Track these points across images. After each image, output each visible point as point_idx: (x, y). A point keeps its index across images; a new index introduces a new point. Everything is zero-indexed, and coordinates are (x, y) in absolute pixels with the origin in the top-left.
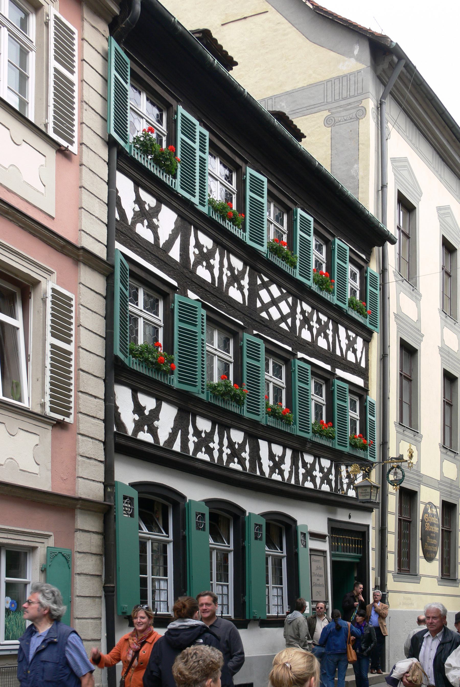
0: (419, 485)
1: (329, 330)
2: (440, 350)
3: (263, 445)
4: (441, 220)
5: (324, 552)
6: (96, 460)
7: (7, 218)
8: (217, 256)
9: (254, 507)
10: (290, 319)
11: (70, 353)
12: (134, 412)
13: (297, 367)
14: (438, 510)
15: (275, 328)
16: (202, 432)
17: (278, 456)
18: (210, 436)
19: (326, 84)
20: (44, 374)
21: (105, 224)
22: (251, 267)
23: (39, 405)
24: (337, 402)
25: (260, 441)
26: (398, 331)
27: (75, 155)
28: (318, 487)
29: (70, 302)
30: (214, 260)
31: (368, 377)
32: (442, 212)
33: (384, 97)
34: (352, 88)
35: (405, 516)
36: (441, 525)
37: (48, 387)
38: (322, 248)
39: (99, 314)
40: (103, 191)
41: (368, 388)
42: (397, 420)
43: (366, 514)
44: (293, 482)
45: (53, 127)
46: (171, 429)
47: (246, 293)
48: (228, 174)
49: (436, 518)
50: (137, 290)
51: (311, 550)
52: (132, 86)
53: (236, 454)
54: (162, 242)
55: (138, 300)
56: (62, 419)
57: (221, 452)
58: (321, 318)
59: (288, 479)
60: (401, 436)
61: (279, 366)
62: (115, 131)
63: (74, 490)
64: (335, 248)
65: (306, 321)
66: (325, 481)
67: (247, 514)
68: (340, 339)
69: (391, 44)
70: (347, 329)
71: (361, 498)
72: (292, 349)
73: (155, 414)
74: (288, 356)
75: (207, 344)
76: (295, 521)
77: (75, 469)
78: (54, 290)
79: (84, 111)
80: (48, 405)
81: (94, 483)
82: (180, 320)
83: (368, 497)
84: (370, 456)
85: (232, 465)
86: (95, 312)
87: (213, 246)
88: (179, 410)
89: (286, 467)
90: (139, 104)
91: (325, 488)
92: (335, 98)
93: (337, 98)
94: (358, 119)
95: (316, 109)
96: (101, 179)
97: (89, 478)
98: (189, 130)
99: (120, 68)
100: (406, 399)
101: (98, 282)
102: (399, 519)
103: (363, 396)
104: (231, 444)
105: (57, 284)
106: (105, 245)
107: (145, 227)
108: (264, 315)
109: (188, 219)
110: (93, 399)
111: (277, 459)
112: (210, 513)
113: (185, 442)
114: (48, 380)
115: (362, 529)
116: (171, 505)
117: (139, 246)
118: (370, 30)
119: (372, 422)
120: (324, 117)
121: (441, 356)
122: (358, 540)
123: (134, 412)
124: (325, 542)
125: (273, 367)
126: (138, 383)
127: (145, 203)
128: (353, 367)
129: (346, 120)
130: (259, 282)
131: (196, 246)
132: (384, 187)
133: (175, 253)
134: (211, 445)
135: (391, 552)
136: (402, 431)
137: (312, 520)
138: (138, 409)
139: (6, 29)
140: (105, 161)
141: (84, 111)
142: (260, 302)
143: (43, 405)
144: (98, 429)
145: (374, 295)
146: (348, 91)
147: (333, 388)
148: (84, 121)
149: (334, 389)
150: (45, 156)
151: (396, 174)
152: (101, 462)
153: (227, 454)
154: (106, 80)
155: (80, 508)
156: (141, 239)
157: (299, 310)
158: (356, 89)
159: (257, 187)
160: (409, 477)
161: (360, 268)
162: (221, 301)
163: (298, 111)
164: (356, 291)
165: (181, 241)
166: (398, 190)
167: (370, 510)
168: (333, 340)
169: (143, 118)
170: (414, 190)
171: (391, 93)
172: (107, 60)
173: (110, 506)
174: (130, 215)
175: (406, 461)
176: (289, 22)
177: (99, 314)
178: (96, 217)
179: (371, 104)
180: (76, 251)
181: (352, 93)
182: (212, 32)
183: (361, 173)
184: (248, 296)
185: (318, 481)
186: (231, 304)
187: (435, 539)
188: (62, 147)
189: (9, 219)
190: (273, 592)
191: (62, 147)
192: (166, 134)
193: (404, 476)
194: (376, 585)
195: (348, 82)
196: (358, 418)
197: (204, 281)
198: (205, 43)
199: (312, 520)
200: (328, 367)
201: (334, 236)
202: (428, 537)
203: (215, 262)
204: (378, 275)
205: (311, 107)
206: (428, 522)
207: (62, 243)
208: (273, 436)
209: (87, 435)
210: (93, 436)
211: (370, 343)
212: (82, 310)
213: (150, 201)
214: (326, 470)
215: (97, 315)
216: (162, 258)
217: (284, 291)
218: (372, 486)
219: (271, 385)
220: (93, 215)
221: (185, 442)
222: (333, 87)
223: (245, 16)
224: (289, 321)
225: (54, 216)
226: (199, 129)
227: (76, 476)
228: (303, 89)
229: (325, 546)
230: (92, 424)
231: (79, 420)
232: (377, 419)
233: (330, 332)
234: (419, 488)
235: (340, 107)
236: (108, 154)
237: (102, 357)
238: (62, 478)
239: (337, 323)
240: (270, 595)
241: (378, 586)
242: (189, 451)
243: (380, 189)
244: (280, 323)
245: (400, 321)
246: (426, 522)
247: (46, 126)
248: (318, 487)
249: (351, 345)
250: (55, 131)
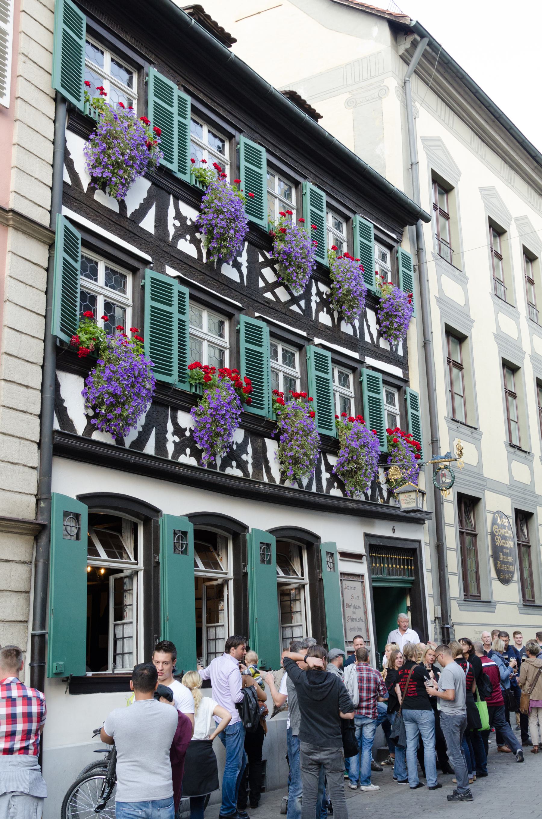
0: (536, 506)
2: (495, 337)
6: (25, 466)
10: (304, 301)
14: (511, 520)
21: (49, 186)
26: (441, 317)
27: (7, 108)
31: (408, 367)
36: (516, 539)
38: (342, 226)
41: (408, 378)
47: (245, 271)
49: (509, 530)
67: (250, 531)
68: (369, 323)
72: (308, 334)
74: (301, 342)
75: (190, 326)
85: (229, 471)
90: (201, 137)
102: (460, 532)
108: (268, 295)
110: (24, 389)
112: (196, 531)
117: (98, 214)
121: (497, 343)
122: (407, 560)
125: (283, 354)
129: (368, 100)
130: (261, 259)
135: (453, 574)
136: (455, 427)
142: (263, 281)
147: (362, 378)
151: (428, 152)
156: (101, 207)
157: (314, 291)
160: (460, 479)
161: (390, 248)
162: (212, 279)
168: (360, 325)
169: (205, 149)
170: (453, 171)
171: (415, 72)
174: (85, 181)
179: (393, 84)
182: (203, 7)
186: (227, 284)
187: (510, 556)
192: (137, 97)
194: (436, 616)
195: (369, 63)
197: (188, 257)
198: (197, 19)
199: (341, 535)
200: (356, 355)
216: (130, 229)
219: (281, 375)
224: (302, 303)
226: (177, 92)
229: (362, 568)
230: (21, 420)
234: (536, 509)
246: (495, 535)
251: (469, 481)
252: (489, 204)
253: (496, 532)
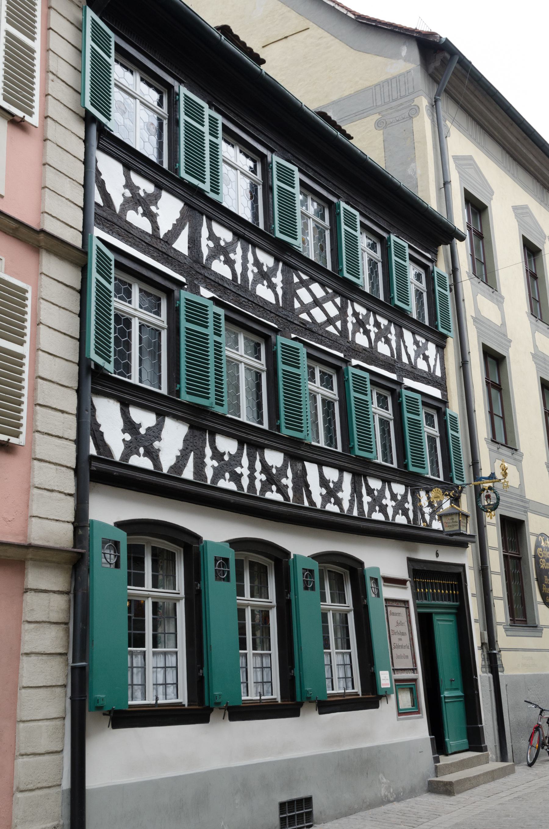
0: (526, 512)
3: (312, 469)
4: (519, 219)
5: (406, 602)
6: (60, 492)
8: (239, 250)
9: (302, 546)
10: (340, 321)
11: (22, 357)
12: (124, 431)
16: (224, 453)
18: (236, 459)
19: (374, 88)
24: (406, 415)
27: (36, 127)
28: (391, 518)
29: (25, 294)
33: (438, 94)
35: (513, 552)
39: (70, 311)
42: (488, 435)
43: (460, 549)
44: (355, 513)
48: (252, 167)
50: (130, 286)
51: (387, 600)
52: (116, 61)
53: (274, 480)
54: (162, 233)
55: (131, 297)
56: (6, 440)
57: (252, 478)
58: (379, 321)
59: (348, 510)
61: (329, 375)
62: (92, 104)
63: (25, 533)
65: (361, 324)
66: (400, 511)
67: (292, 557)
68: (406, 344)
69: (440, 41)
70: (413, 333)
71: (447, 529)
72: (345, 356)
73: (155, 432)
76: (361, 564)
77: (28, 506)
79: (50, 82)
83: (457, 528)
84: (457, 479)
85: (269, 495)
88: (190, 428)
89: (345, 494)
91: (401, 519)
92: (385, 101)
93: (387, 100)
94: (411, 118)
95: (365, 114)
96: (75, 157)
97: (49, 517)
98: (195, 112)
99: (99, 38)
100: (498, 411)
101: (70, 275)
102: (504, 555)
103: (173, 291)
104: (266, 469)
105: (5, 273)
106: (80, 232)
107: (140, 215)
108: (304, 316)
110: (60, 414)
111: (331, 485)
113: (200, 466)
115: (456, 570)
117: (130, 236)
118: (416, 29)
119: (456, 439)
120: (375, 121)
121: (535, 363)
122: (452, 584)
124: (406, 588)
127: (138, 188)
128: (425, 375)
129: (398, 121)
130: (296, 280)
132: (446, 183)
133: (181, 245)
136: (495, 449)
137: (385, 561)
140: (80, 138)
141: (50, 82)
142: (299, 302)
144: (68, 454)
146: (399, 92)
147: (401, 399)
148: (50, 92)
149: (402, 401)
152: (70, 495)
157: (350, 311)
158: (407, 89)
159: (286, 176)
163: (346, 118)
165: (189, 232)
166: (464, 188)
167: (463, 545)
168: (397, 346)
171: (446, 91)
172: (81, 31)
173: (82, 555)
175: (500, 480)
176: (332, 35)
177: (70, 311)
178: (67, 199)
179: (424, 102)
180: (34, 235)
182: (232, 28)
183: (419, 172)
185: (390, 511)
186: (261, 305)
188: (15, 118)
191: (15, 118)
192: (167, 117)
193: (498, 499)
194: (483, 642)
195: (398, 83)
196: (438, 434)
197: (223, 278)
199: (385, 561)
200: (394, 376)
202: (546, 577)
204: (446, 275)
205: (360, 113)
206: (543, 558)
207: (14, 225)
209: (47, 459)
210: (57, 462)
211: (445, 350)
213: (146, 187)
214: (399, 498)
216: (164, 250)
217: (330, 291)
220: (62, 196)
221: (200, 466)
222: (382, 90)
223: (286, 36)
226: (208, 111)
227: (29, 515)
228: (350, 97)
229: (406, 594)
230: (56, 446)
231: (35, 441)
232: (462, 434)
234: (527, 516)
236: (84, 130)
237: (74, 363)
238: (5, 519)
240: (333, 664)
241: (486, 643)
242: (206, 478)
244: (327, 327)
246: (540, 558)
248: (391, 518)
251: (512, 503)
252: (523, 223)
253: (541, 555)
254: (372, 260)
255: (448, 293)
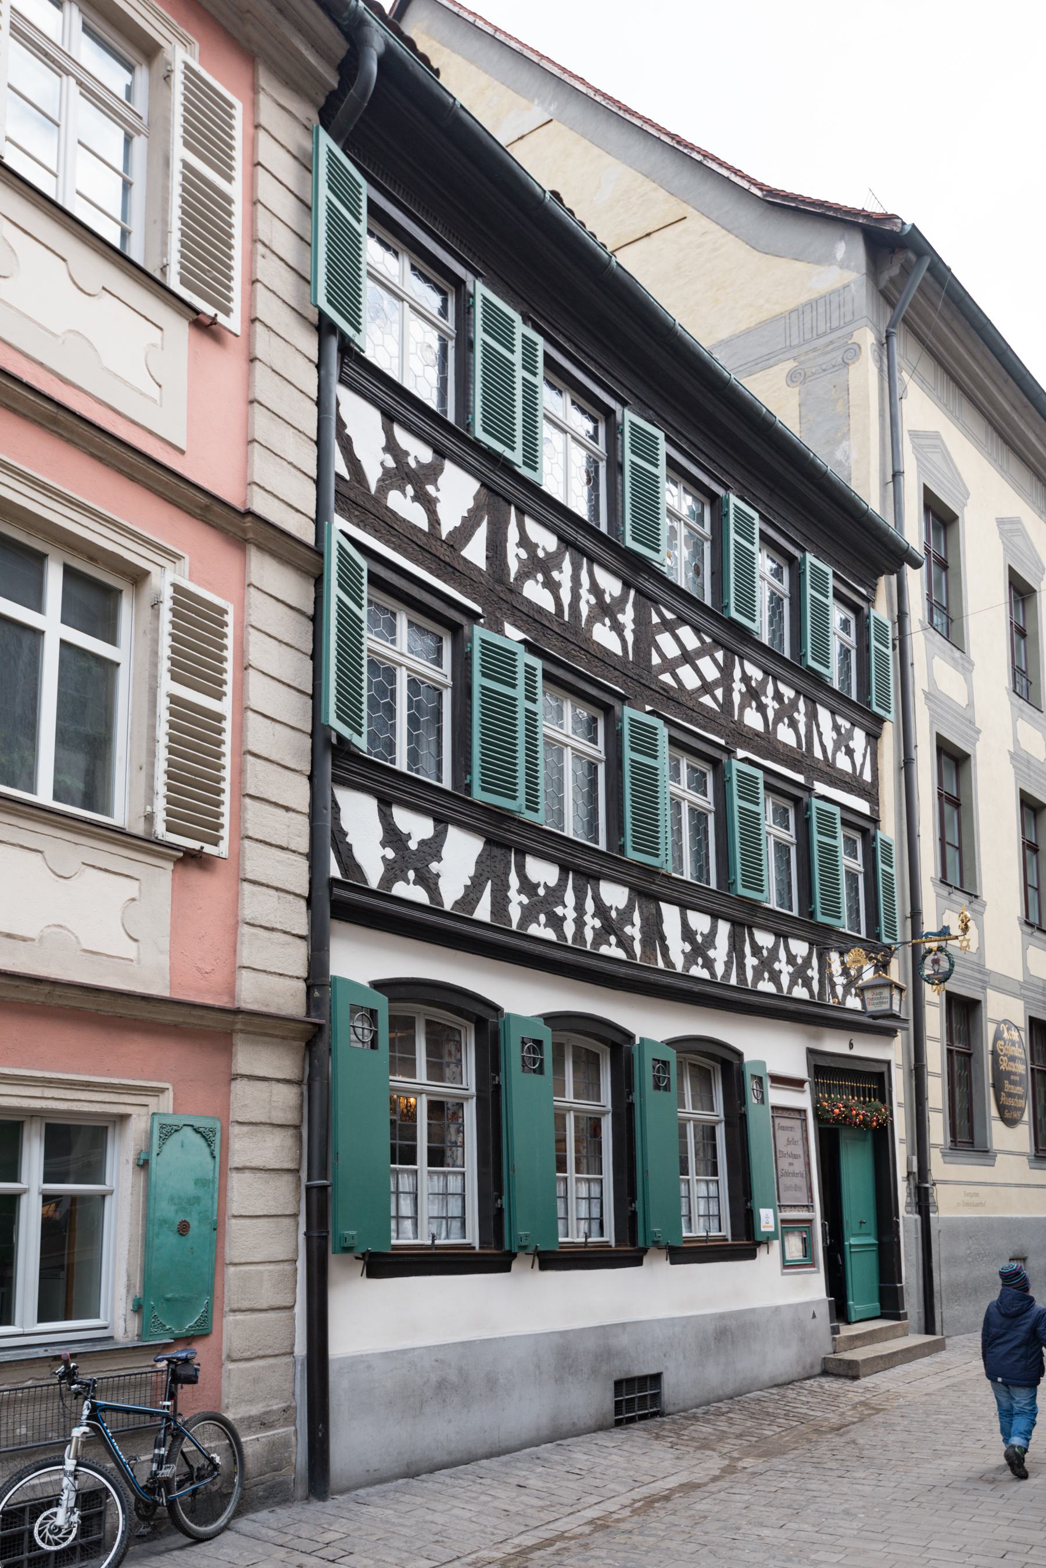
0: (984, 988)
1: (799, 712)
3: (670, 914)
5: (802, 1112)
7: (56, 432)
8: (567, 565)
11: (220, 718)
12: (384, 844)
13: (734, 772)
15: (690, 704)
17: (702, 934)
18: (555, 895)
20: (152, 754)
22: (639, 591)
23: (143, 819)
25: (663, 905)
28: (785, 990)
30: (561, 572)
32: (1007, 527)
33: (892, 324)
34: (835, 316)
37: (161, 780)
40: (308, 418)
42: (936, 874)
44: (733, 981)
45: (180, 273)
46: (470, 878)
47: (630, 637)
50: (394, 615)
54: (445, 530)
57: (580, 923)
59: (723, 977)
60: (945, 903)
64: (805, 570)
65: (753, 694)
67: (637, 1042)
69: (902, 229)
71: (870, 1008)
72: (727, 743)
73: (433, 848)
76: (739, 1055)
78: (177, 588)
80: (161, 817)
81: (281, 979)
82: (484, 675)
83: (886, 1007)
86: (287, 644)
87: (558, 548)
89: (720, 953)
91: (800, 992)
92: (804, 332)
96: (302, 392)
99: (339, 183)
101: (290, 586)
102: (948, 1050)
107: (409, 499)
108: (666, 678)
109: (502, 493)
110: (281, 812)
111: (699, 939)
114: (161, 766)
115: (876, 1068)
116: (473, 1026)
118: (863, 210)
119: (889, 877)
120: (787, 371)
121: (1014, 767)
122: (870, 1089)
123: (384, 844)
126: (391, 789)
128: (849, 780)
130: (655, 619)
131: (520, 544)
132: (897, 475)
134: (559, 911)
136: (946, 894)
137: (774, 1051)
138: (393, 837)
139: (72, 81)
142: (660, 656)
143: (149, 818)
145: (882, 657)
150: (161, 329)
153: (593, 928)
154: (308, 207)
155: (242, 1031)
157: (737, 674)
161: (856, 609)
164: (849, 651)
171: (905, 320)
173: (320, 1027)
174: (373, 475)
175: (956, 938)
178: (290, 463)
179: (867, 338)
180: (237, 519)
181: (835, 324)
183: (854, 455)
184: (634, 643)
185: (785, 980)
189: (61, 435)
190: (700, 1190)
191: (201, 316)
192: (454, 335)
196: (861, 869)
197: (540, 610)
199: (774, 1051)
200: (800, 778)
201: (803, 550)
203: (564, 576)
204: (889, 624)
206: (1004, 1055)
208: (687, 898)
209: (264, 882)
210: (280, 886)
212: (254, 636)
213: (419, 452)
215: (293, 651)
216: (447, 559)
217: (708, 640)
218: (891, 985)
223: (648, 231)
225: (184, 448)
226: (521, 329)
228: (748, 332)
229: (803, 1100)
230: (278, 861)
232: (898, 871)
233: (801, 718)
235: (815, 350)
238: (199, 969)
239: (814, 702)
242: (510, 921)
243: (890, 479)
245: (936, 704)
247: (163, 269)
248: (785, 990)
249: (843, 741)
250: (184, 282)
254: (775, 594)
255: (889, 652)
